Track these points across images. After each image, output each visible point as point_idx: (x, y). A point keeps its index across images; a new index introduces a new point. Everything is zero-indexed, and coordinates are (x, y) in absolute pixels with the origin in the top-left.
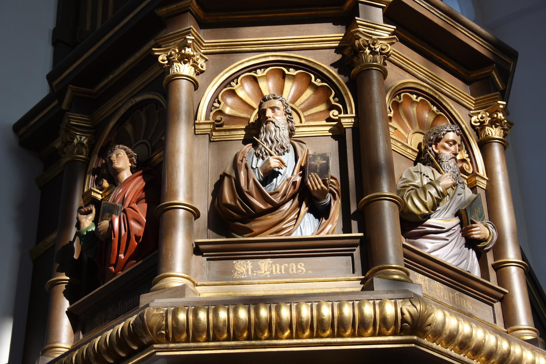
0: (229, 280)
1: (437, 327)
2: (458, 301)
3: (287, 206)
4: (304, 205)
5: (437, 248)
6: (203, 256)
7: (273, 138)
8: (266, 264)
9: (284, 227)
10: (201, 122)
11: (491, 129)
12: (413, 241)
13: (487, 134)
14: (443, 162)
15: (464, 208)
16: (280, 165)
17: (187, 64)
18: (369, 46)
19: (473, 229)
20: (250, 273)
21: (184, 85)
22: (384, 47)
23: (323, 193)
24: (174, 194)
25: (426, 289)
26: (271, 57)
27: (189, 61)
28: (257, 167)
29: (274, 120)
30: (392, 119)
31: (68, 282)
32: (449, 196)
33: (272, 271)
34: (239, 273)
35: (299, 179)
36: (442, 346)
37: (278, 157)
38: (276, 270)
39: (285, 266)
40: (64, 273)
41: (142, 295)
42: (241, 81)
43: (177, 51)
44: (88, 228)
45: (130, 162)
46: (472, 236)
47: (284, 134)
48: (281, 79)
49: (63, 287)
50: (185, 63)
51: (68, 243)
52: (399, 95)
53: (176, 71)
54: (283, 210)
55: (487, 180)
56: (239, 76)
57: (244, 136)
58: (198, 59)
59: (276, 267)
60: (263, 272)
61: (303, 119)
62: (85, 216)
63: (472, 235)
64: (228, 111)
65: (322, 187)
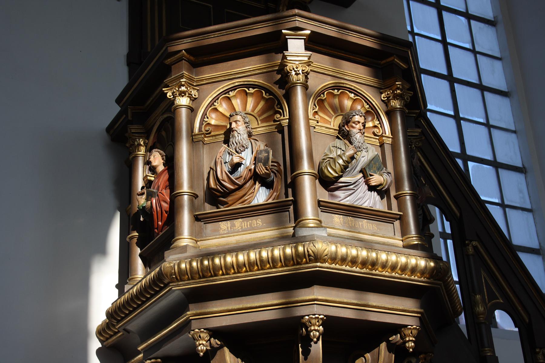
0: (217, 235)
1: (332, 256)
2: (365, 226)
3: (248, 185)
4: (257, 183)
5: (347, 196)
6: (201, 222)
7: (237, 141)
8: (239, 222)
9: (246, 198)
10: (196, 134)
11: (394, 101)
12: (332, 194)
13: (392, 105)
14: (352, 136)
15: (364, 167)
16: (240, 160)
17: (184, 97)
18: (293, 69)
19: (371, 180)
20: (229, 229)
21: (184, 113)
22: (304, 69)
23: (268, 175)
24: (181, 187)
25: (341, 224)
26: (237, 82)
27: (185, 94)
28: (229, 162)
29: (236, 129)
30: (318, 112)
31: (138, 236)
32: (356, 159)
33: (242, 226)
34: (223, 230)
35: (253, 167)
36: (339, 265)
37: (239, 155)
38: (244, 226)
39: (250, 222)
40: (136, 231)
41: (165, 252)
42: (220, 101)
43: (177, 89)
44: (143, 204)
45: (163, 160)
46: (371, 184)
47: (244, 137)
48: (245, 95)
49: (135, 240)
50: (183, 96)
51: (136, 211)
52: (323, 94)
53: (178, 102)
54: (246, 187)
55: (391, 137)
56: (219, 98)
57: (224, 138)
58: (191, 91)
59: (244, 224)
60: (237, 228)
61: (259, 122)
62: (141, 196)
63: (371, 183)
64: (213, 122)
65: (265, 172)
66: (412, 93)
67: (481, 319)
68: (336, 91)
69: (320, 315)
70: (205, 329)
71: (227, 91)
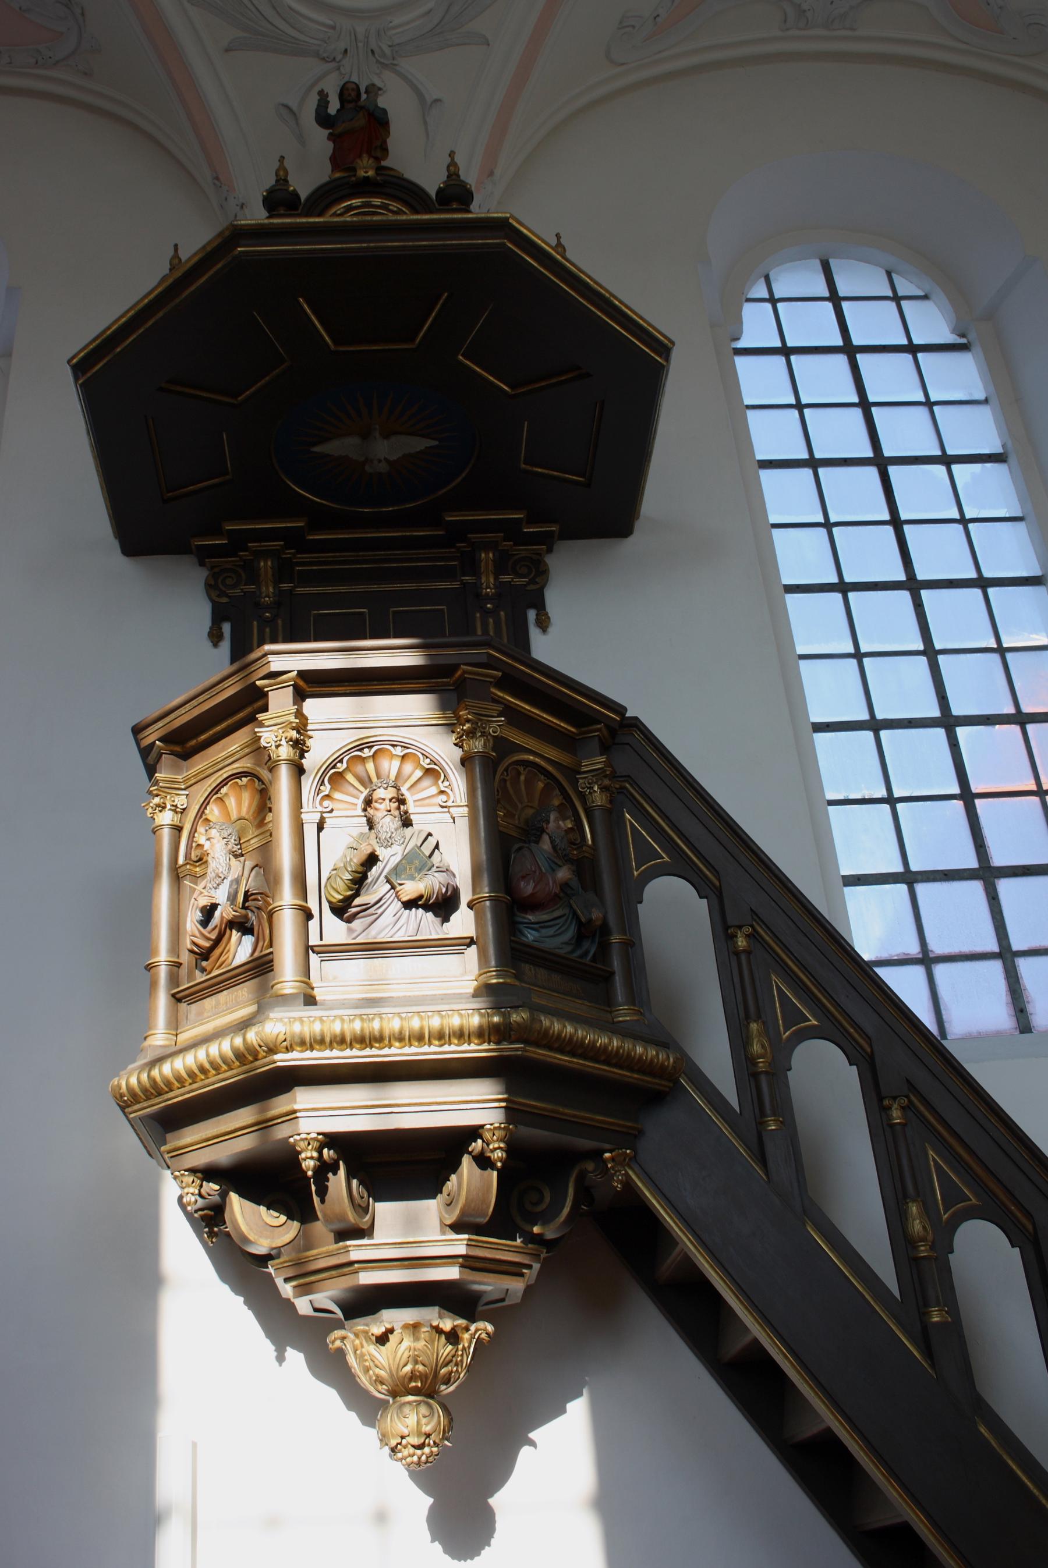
30: (331, 795)
66: (503, 719)
67: (761, 1065)
68: (366, 750)
69: (308, 1134)
70: (185, 1171)
71: (217, 790)
